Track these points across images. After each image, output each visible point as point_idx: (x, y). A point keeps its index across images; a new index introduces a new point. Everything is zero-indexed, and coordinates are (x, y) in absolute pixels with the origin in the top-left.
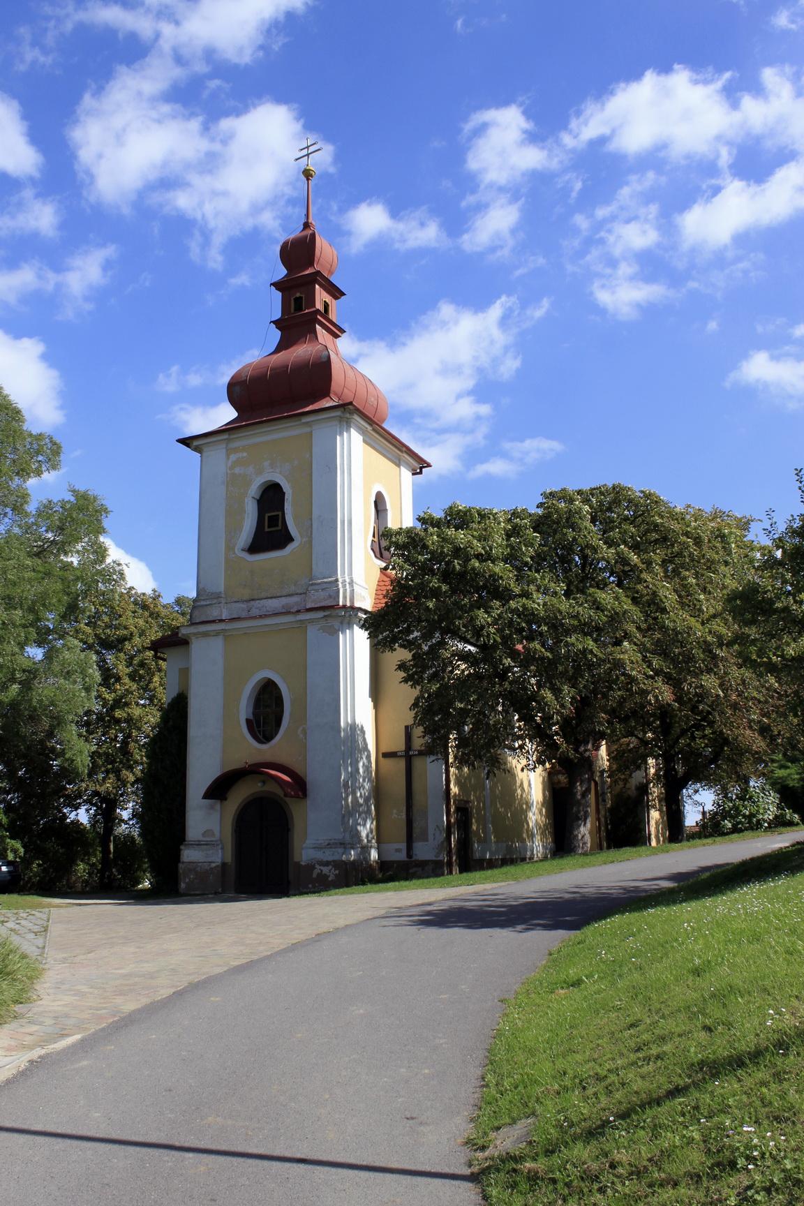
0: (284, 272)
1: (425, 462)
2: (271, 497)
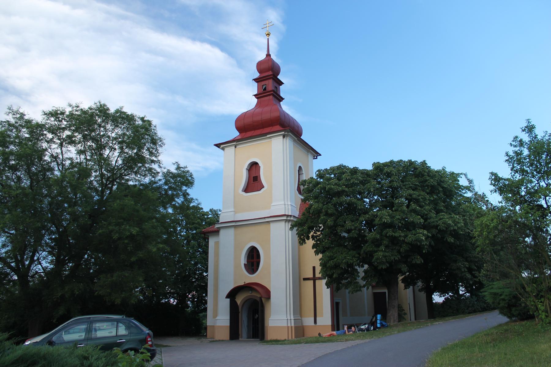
0: (259, 74)
1: (318, 153)
2: (254, 166)
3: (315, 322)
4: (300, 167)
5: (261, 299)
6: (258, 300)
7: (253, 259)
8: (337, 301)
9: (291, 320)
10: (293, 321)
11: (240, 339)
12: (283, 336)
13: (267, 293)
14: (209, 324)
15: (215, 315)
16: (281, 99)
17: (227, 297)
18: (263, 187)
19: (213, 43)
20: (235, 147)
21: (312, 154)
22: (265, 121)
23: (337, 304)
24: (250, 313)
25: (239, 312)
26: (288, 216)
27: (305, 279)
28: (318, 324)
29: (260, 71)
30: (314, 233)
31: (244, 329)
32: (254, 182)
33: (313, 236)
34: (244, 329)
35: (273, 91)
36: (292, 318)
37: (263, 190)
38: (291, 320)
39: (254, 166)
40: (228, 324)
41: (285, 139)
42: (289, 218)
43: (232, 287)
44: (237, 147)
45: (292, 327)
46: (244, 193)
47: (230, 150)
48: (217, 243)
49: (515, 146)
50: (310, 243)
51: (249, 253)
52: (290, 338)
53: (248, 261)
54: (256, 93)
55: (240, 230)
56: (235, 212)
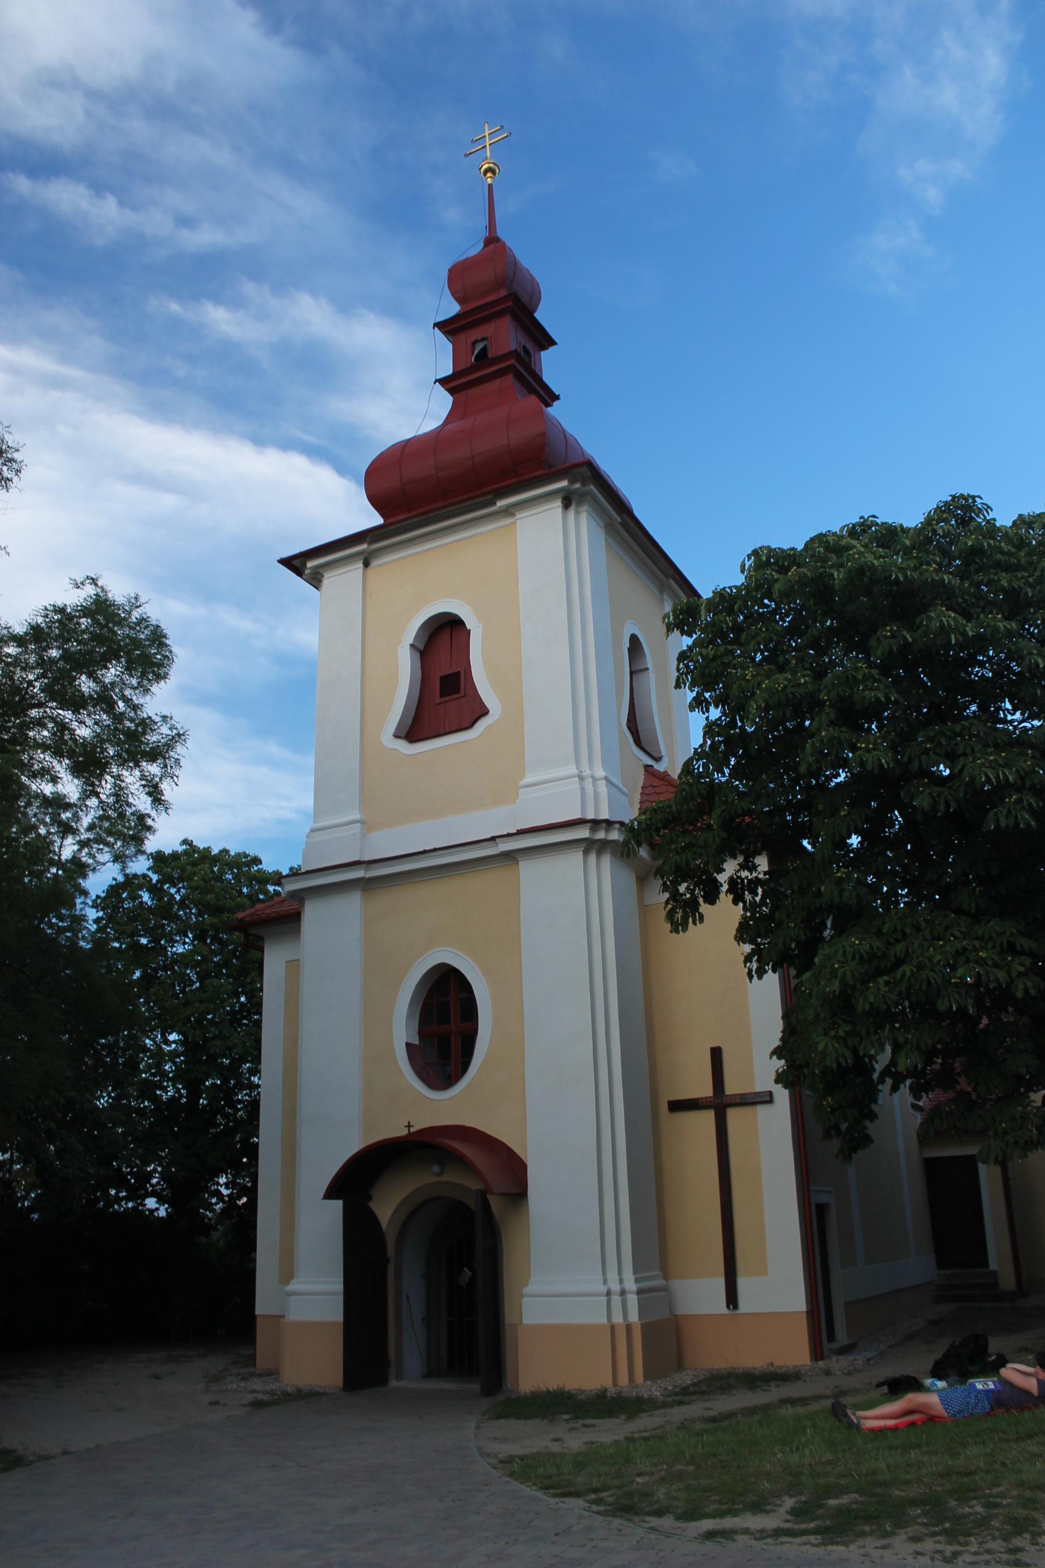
2: (444, 635)
3: (732, 1298)
4: (634, 640)
5: (483, 1196)
6: (471, 1203)
7: (446, 1022)
8: (822, 1199)
9: (623, 1293)
10: (633, 1300)
11: (393, 1383)
12: (590, 1375)
13: (514, 1168)
14: (261, 1308)
15: (287, 1274)
16: (549, 397)
17: (329, 1195)
18: (485, 712)
19: (314, 452)
20: (366, 564)
22: (489, 450)
23: (822, 1209)
24: (438, 1227)
25: (387, 1261)
27: (678, 1106)
28: (746, 1305)
30: (742, 867)
31: (409, 1340)
32: (444, 690)
33: (734, 884)
34: (409, 1340)
35: (514, 354)
36: (631, 1285)
37: (482, 724)
38: (623, 1293)
39: (444, 635)
40: (334, 1312)
41: (571, 512)
42: (601, 835)
43: (355, 1145)
44: (375, 563)
45: (629, 1327)
46: (403, 747)
47: (345, 581)
48: (294, 968)
50: (724, 915)
52: (624, 1380)
53: (421, 1034)
55: (388, 900)
56: (366, 825)
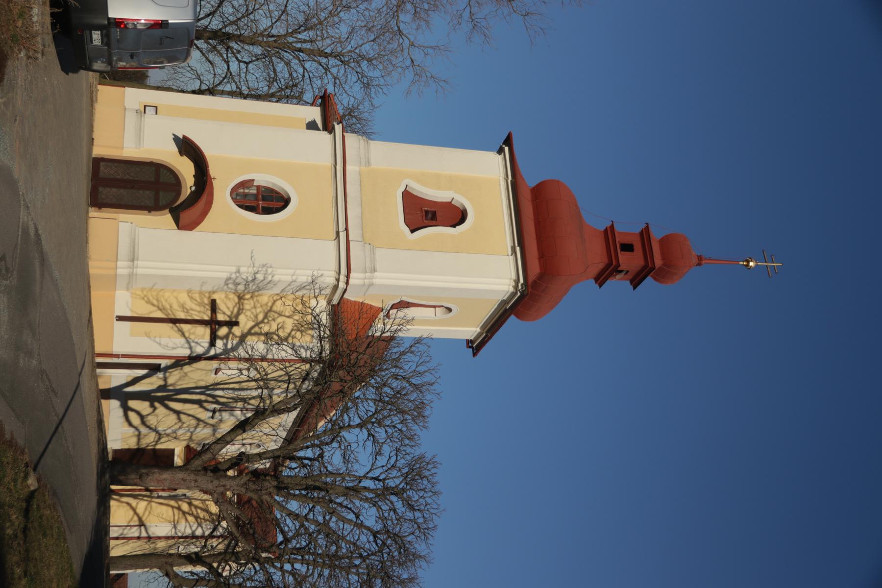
3: (121, 318)
7: (267, 201)
16: (601, 279)
21: (479, 335)
26: (348, 277)
29: (665, 242)
49: (191, 298)
51: (277, 193)
54: (618, 228)
